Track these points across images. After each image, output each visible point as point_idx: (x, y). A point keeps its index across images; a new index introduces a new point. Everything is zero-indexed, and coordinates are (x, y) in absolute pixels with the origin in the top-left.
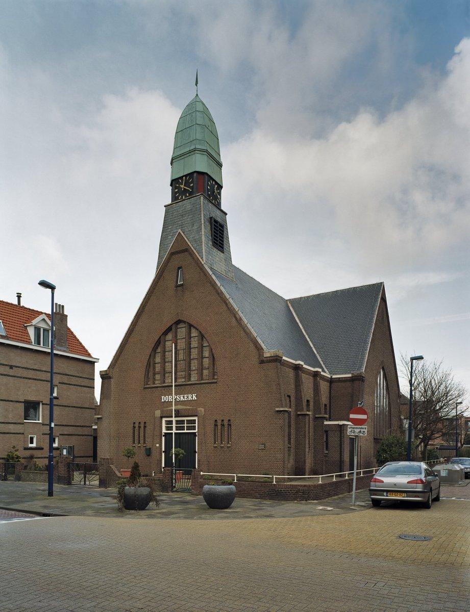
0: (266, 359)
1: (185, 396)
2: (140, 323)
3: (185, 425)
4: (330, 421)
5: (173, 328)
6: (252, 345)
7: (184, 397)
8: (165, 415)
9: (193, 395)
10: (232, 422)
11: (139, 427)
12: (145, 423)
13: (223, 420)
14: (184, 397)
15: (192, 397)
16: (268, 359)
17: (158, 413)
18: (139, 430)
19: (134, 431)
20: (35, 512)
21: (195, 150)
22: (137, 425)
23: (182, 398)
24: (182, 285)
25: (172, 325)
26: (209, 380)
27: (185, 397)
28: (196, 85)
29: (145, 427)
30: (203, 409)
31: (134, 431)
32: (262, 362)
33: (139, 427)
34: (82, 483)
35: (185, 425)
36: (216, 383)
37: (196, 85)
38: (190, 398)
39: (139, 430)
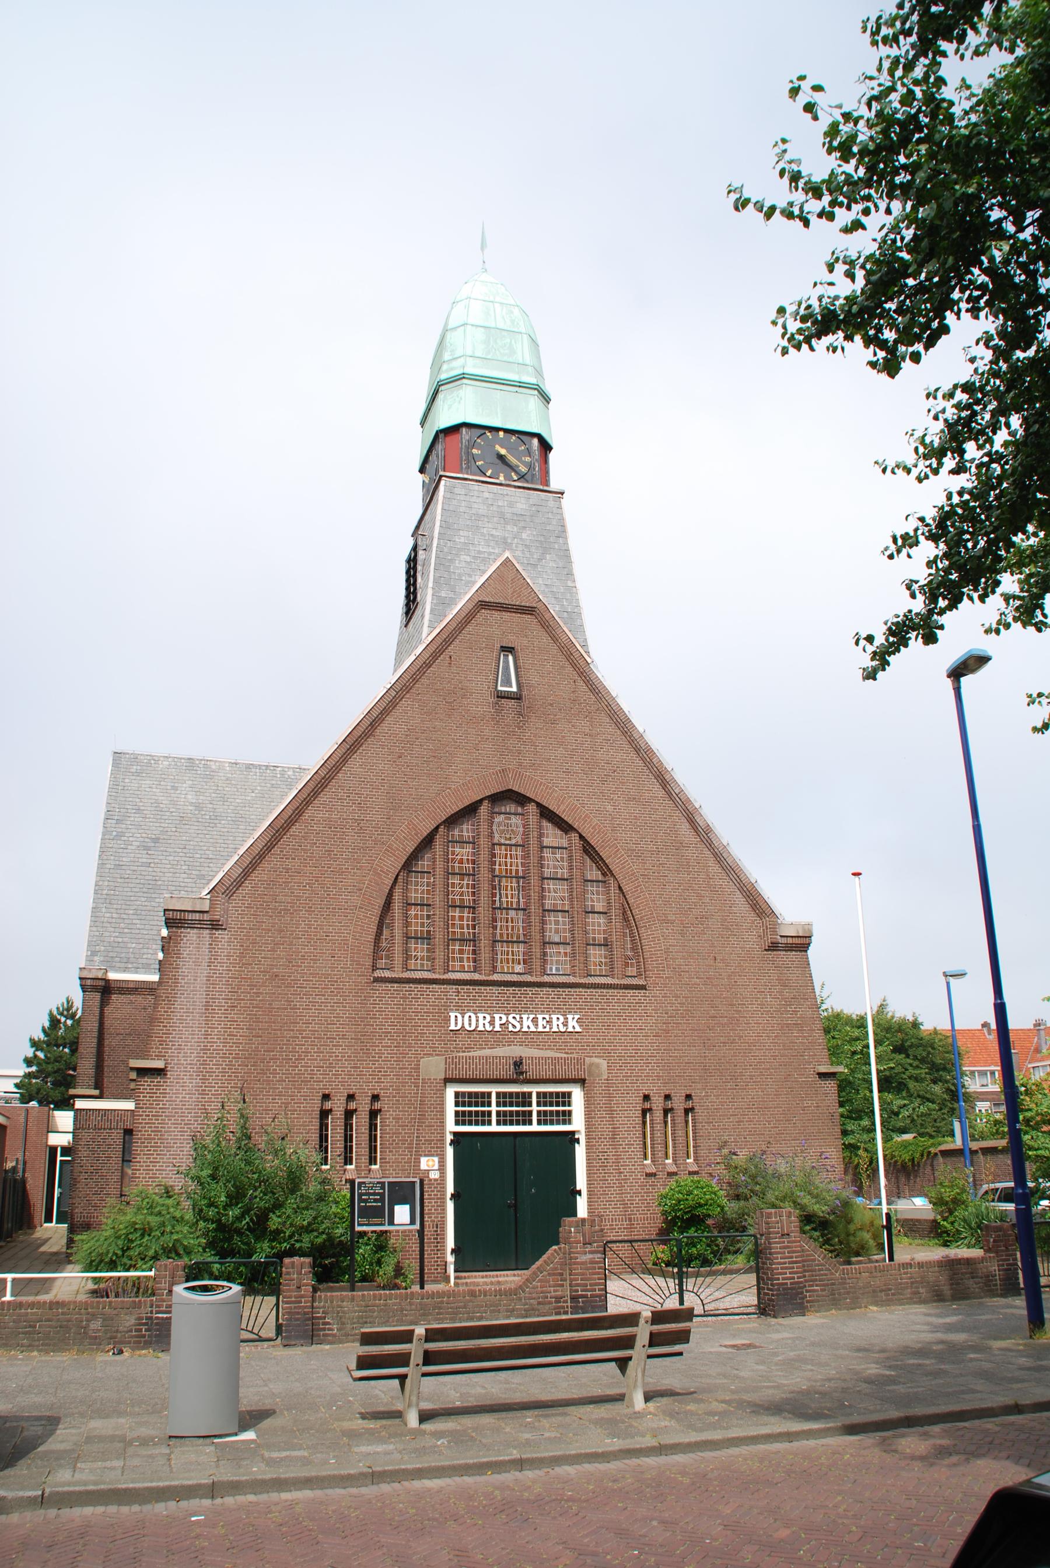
0: (784, 940)
1: (540, 1017)
2: (355, 763)
3: (494, 1108)
4: (880, 1110)
5: (484, 809)
6: (739, 898)
7: (535, 1021)
8: (456, 1074)
9: (570, 1017)
10: (696, 1102)
11: (349, 1114)
12: (375, 1098)
13: (667, 1097)
14: (535, 1021)
15: (565, 1024)
16: (790, 941)
17: (434, 1067)
18: (348, 1126)
19: (323, 1126)
20: (383, 1413)
21: (462, 377)
22: (338, 1106)
23: (526, 1023)
24: (517, 697)
25: (481, 801)
26: (574, 974)
27: (541, 1022)
28: (483, 247)
29: (374, 1114)
30: (603, 1064)
31: (323, 1126)
32: (774, 947)
33: (349, 1114)
34: (246, 1335)
35: (494, 1108)
36: (643, 987)
37: (482, 249)
38: (558, 1024)
39: (348, 1126)
